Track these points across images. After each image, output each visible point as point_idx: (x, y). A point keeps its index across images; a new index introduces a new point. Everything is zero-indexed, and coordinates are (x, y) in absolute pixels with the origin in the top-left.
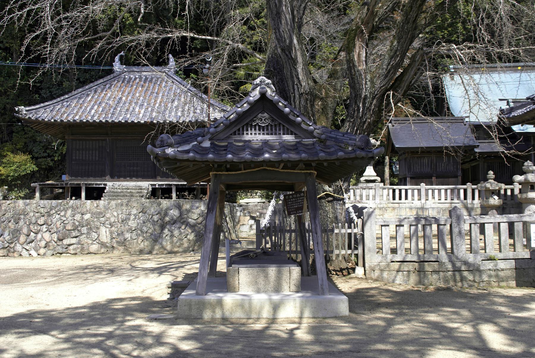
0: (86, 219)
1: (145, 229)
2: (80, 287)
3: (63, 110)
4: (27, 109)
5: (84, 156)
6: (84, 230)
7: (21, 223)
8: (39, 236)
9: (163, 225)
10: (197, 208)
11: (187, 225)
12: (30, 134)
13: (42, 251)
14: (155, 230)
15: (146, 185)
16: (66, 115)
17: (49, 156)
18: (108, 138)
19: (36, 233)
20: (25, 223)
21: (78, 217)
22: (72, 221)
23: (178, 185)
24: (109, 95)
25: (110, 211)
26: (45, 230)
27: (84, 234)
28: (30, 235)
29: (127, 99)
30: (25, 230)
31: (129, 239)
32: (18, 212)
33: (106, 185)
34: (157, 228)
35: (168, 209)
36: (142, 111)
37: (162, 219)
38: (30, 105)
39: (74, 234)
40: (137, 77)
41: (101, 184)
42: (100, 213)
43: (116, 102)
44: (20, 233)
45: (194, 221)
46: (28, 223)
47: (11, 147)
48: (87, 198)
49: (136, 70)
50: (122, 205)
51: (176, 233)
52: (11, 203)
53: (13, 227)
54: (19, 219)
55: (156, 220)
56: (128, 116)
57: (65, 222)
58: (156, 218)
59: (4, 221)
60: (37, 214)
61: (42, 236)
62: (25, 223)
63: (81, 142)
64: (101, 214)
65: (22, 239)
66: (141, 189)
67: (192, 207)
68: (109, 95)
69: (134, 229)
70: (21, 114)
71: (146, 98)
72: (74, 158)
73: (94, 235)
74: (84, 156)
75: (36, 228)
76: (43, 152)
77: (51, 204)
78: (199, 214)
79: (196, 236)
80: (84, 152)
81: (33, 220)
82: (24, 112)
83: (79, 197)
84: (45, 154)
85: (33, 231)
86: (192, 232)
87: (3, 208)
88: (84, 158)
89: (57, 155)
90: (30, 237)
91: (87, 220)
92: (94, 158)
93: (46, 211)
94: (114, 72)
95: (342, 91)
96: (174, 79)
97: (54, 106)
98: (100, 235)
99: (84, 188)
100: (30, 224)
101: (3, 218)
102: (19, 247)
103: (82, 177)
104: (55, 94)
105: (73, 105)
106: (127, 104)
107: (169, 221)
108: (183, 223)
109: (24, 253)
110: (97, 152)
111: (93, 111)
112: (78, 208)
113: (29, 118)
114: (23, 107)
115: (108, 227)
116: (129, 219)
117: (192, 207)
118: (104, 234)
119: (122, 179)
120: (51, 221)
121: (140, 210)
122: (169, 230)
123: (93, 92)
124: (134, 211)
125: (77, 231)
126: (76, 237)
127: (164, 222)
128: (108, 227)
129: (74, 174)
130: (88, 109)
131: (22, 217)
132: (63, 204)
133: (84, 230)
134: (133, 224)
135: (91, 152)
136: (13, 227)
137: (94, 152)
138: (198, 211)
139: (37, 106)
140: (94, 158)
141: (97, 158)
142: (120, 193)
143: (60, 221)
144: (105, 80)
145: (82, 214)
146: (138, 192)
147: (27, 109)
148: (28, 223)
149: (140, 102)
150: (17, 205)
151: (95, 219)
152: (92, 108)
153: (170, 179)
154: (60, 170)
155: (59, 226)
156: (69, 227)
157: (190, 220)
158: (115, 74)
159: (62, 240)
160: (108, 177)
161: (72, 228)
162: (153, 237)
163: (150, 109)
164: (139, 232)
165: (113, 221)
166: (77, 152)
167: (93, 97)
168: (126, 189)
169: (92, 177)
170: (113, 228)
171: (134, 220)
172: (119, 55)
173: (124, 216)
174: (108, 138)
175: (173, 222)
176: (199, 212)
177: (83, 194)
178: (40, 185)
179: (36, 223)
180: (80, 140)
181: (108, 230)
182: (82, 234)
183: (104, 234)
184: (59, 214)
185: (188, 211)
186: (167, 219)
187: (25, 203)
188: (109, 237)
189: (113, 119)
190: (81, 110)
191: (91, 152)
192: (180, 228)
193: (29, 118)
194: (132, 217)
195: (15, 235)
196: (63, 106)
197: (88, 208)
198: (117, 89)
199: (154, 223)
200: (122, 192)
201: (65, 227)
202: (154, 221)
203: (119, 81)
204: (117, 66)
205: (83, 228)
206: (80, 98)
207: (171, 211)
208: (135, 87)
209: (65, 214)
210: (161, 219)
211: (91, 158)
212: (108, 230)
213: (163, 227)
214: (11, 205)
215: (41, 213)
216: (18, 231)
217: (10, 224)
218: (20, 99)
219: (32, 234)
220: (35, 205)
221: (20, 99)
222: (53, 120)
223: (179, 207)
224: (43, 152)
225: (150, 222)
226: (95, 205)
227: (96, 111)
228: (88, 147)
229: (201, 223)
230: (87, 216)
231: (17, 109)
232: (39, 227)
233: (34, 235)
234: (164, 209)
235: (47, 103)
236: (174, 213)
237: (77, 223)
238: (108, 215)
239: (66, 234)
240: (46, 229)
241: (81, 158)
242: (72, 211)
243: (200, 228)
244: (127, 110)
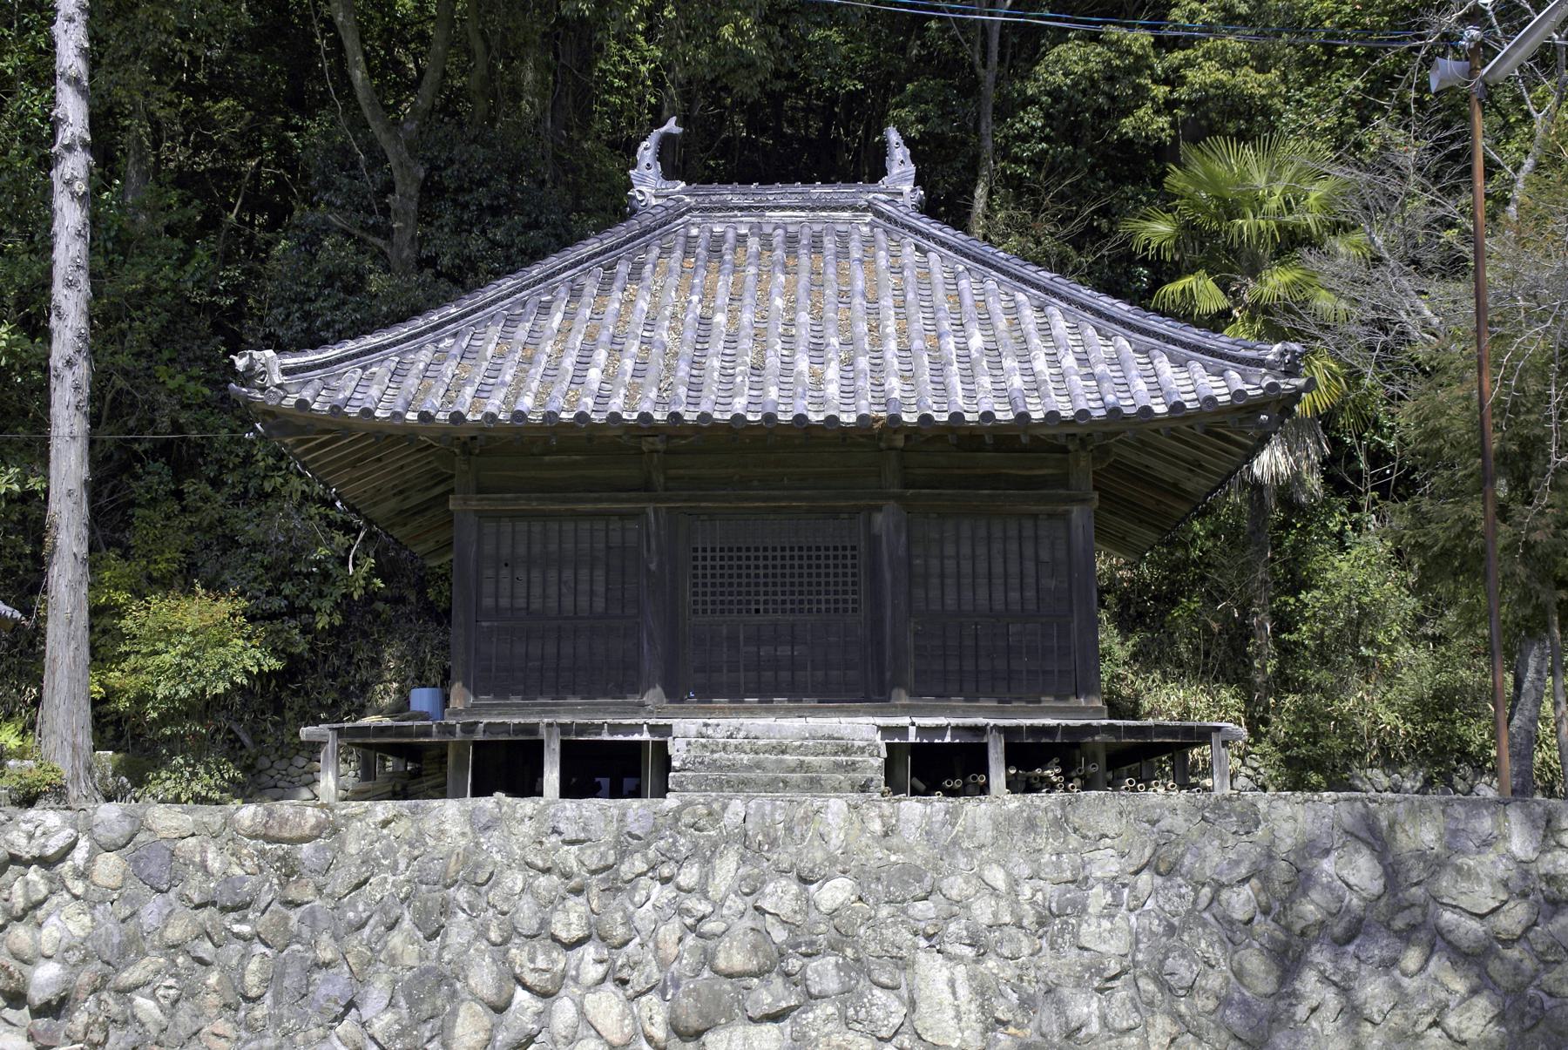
0: (825, 906)
1: (1182, 970)
3: (449, 368)
4: (290, 361)
5: (537, 590)
6: (824, 973)
7: (459, 931)
8: (564, 1011)
9: (1287, 946)
10: (1486, 843)
11: (1431, 950)
12: (211, 513)
14: (1239, 974)
15: (861, 729)
16: (469, 391)
17: (292, 612)
18: (650, 508)
19: (544, 995)
20: (482, 934)
22: (747, 922)
23: (1019, 728)
24: (643, 305)
25: (962, 861)
26: (593, 972)
27: (822, 996)
28: (508, 1004)
29: (733, 318)
30: (483, 977)
31: (1095, 1027)
32: (437, 866)
33: (667, 730)
34: (1255, 962)
35: (1311, 849)
36: (833, 372)
37: (1276, 906)
38: (299, 347)
39: (768, 996)
40: (743, 230)
41: (637, 728)
42: (911, 873)
43: (690, 335)
44: (454, 994)
45: (1474, 924)
46: (494, 935)
47: (124, 567)
48: (567, 791)
49: (736, 200)
50: (1031, 825)
51: (1373, 991)
52: (398, 817)
53: (410, 955)
54: (446, 909)
55: (1240, 914)
56: (773, 393)
57: (709, 927)
58: (1240, 901)
59: (361, 926)
60: (543, 881)
61: (582, 1013)
62: (482, 934)
63: (522, 526)
64: (912, 881)
66: (846, 750)
67: (1453, 839)
68: (643, 305)
69: (1114, 968)
70: (263, 389)
71: (848, 315)
72: (488, 602)
74: (537, 590)
75: (541, 962)
76: (269, 593)
77: (622, 818)
78: (1505, 884)
79: (1500, 1018)
80: (536, 575)
81: (527, 918)
82: (278, 379)
83: (532, 788)
84: (277, 603)
85: (530, 978)
86: (1474, 992)
87: (352, 848)
88: (536, 605)
89: (327, 604)
90: (509, 1015)
91: (832, 914)
92: (583, 601)
93: (594, 863)
94: (634, 211)
96: (928, 236)
97: (402, 353)
98: (923, 1007)
99: (556, 746)
100: (506, 941)
101: (353, 905)
103: (526, 694)
104: (328, 325)
105: (491, 348)
106: (746, 344)
107: (1322, 924)
108: (1406, 936)
110: (600, 574)
111: (594, 375)
112: (773, 843)
113: (302, 404)
114: (270, 353)
115: (959, 959)
116: (1081, 909)
117: (1453, 839)
119: (722, 702)
120: (628, 920)
121: (1138, 858)
122: (1325, 979)
123: (563, 292)
124: (1106, 863)
125: (777, 982)
126: (776, 1017)
127: (1287, 929)
128: (959, 959)
129: (496, 682)
130: (569, 363)
131: (462, 895)
132: (687, 819)
134: (1106, 937)
135: (568, 574)
136: (410, 955)
137: (584, 573)
138: (1491, 865)
139: (332, 353)
140: (583, 601)
141: (600, 605)
142: (749, 768)
143: (676, 923)
144: (608, 243)
145: (804, 881)
146: (838, 767)
147: (290, 361)
148: (494, 935)
149: (803, 333)
150: (430, 825)
151: (884, 911)
152: (584, 362)
153: (957, 702)
154: (334, 675)
155: (672, 950)
156: (734, 957)
157: (1448, 916)
158: (634, 225)
159: (698, 1034)
160: (654, 696)
161: (753, 965)
162: (1233, 1017)
163: (863, 363)
164: (1147, 986)
165: (985, 919)
166: (505, 572)
167: (569, 316)
168: (772, 749)
169: (574, 693)
170: (991, 963)
171: (1109, 913)
172: (656, 134)
173: (1048, 887)
174: (650, 508)
175: (1350, 931)
176: (1501, 871)
177: (552, 777)
178: (340, 733)
179: (543, 934)
180: (514, 516)
181: (961, 971)
182: (812, 997)
184: (665, 881)
185: (1436, 864)
186: (1310, 909)
187: (471, 818)
188: (973, 1016)
189: (705, 407)
190: (537, 372)
191: (568, 574)
192: (1390, 964)
193: (302, 404)
194: (1098, 898)
195: (426, 1009)
196: (441, 356)
197: (836, 839)
198: (673, 281)
199: (1233, 932)
200: (758, 765)
201: (708, 958)
202: (1227, 922)
203: (670, 251)
204: (648, 182)
205: (814, 964)
206: (511, 321)
207: (1327, 865)
208: (752, 270)
209: (705, 879)
210: (1266, 912)
211: (568, 602)
212: (961, 971)
213: (1287, 960)
214: (399, 828)
215: (567, 876)
216: (442, 979)
217: (396, 940)
218: (166, 354)
219: (521, 995)
220: (528, 828)
221: (166, 354)
222: (411, 416)
223: (1373, 837)
224: (269, 593)
225: (1205, 924)
226: (877, 826)
227: (609, 377)
228: (553, 547)
229: (1523, 936)
230: (835, 893)
231: (241, 363)
232: (561, 960)
233: (535, 1004)
234: (1285, 845)
235: (370, 341)
236: (1359, 873)
237: (779, 935)
238: (956, 886)
239: (717, 997)
240: (601, 969)
241: (521, 603)
242: (743, 860)
243: (1517, 968)
244: (757, 369)
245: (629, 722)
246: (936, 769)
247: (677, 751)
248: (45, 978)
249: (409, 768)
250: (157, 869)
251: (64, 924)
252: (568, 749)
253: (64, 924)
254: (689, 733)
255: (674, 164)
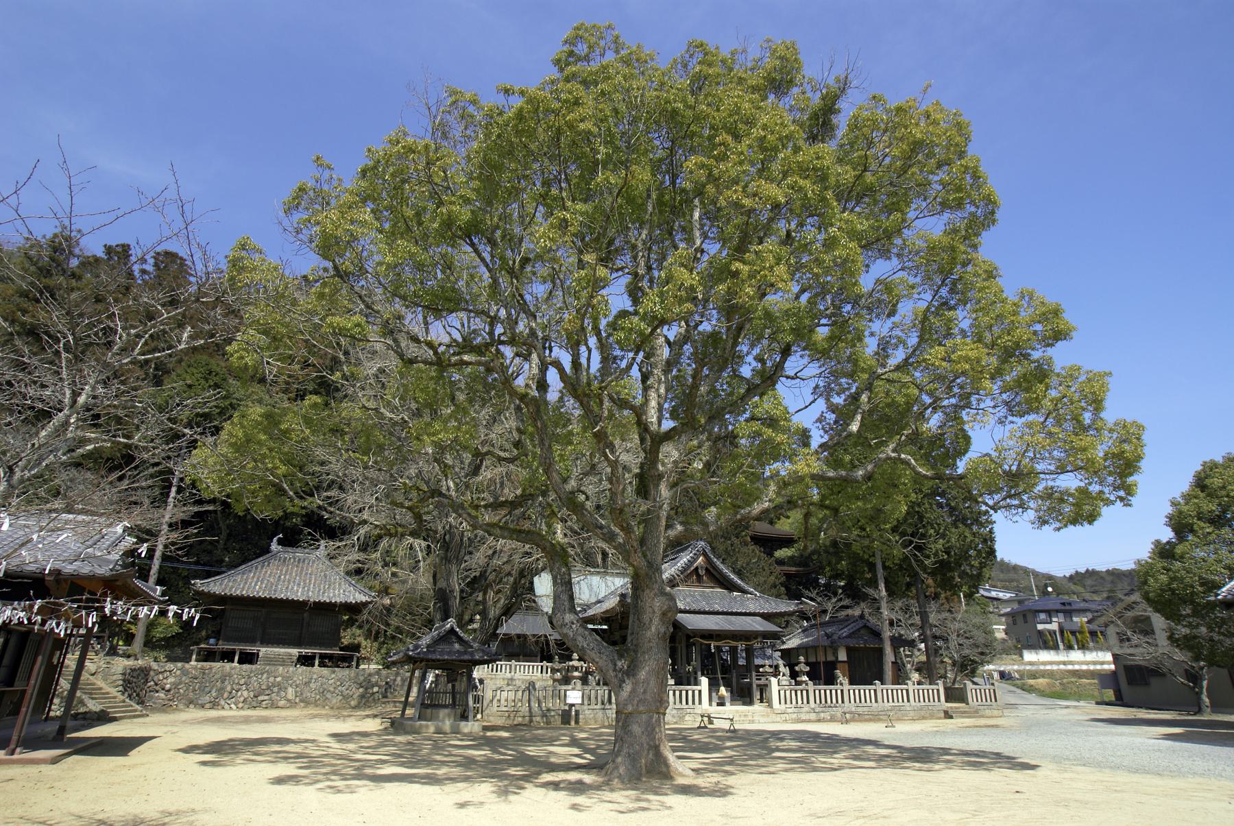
2: (204, 763)
6: (276, 689)
13: (240, 705)
15: (295, 652)
21: (271, 679)
30: (229, 688)
65: (226, 695)
73: (283, 694)
95: (710, 99)
102: (222, 702)
109: (227, 706)
118: (291, 692)
129: (228, 640)
133: (276, 689)
177: (236, 658)
183: (291, 692)
204: (274, 546)
230: (279, 679)
245: (254, 649)
246: (306, 661)
247: (261, 654)
248: (168, 687)
249: (209, 656)
250: (185, 672)
251: (171, 680)
252: (241, 653)
253: (171, 680)
254: (263, 651)
255: (280, 542)
